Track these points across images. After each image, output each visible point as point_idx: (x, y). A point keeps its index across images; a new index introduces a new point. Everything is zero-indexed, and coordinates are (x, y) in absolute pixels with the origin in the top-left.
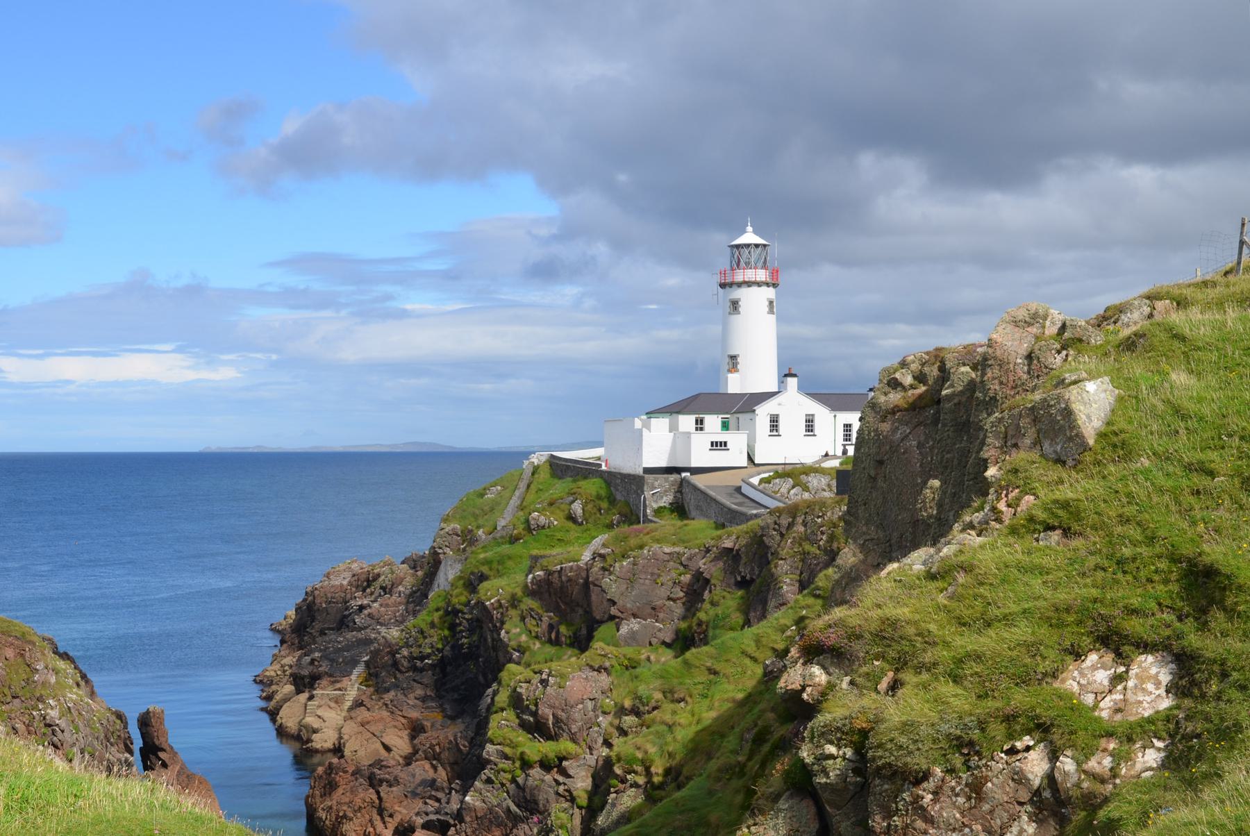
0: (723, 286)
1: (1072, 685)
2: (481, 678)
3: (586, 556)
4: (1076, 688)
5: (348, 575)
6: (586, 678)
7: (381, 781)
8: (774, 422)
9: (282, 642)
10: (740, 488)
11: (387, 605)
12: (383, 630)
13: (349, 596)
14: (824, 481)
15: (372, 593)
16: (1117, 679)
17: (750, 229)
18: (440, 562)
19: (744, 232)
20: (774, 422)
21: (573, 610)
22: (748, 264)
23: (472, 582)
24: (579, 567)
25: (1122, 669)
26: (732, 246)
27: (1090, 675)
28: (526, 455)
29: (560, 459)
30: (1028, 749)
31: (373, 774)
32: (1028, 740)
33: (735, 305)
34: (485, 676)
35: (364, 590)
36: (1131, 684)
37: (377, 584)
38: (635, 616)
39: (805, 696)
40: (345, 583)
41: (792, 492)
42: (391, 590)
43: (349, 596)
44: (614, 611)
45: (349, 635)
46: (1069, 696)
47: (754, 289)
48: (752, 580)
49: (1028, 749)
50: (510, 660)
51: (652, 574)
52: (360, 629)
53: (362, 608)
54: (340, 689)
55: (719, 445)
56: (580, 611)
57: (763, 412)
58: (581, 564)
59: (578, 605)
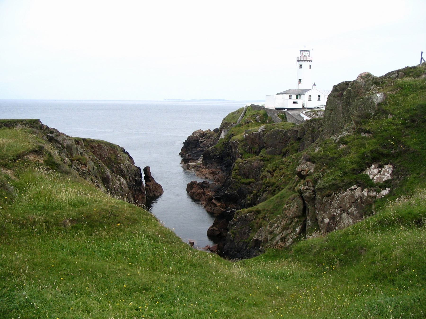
0: (298, 61)
1: (368, 173)
2: (231, 161)
3: (259, 131)
4: (368, 174)
7: (205, 187)
9: (225, 144)
11: (208, 142)
12: (207, 148)
14: (322, 113)
16: (379, 172)
23: (229, 137)
25: (380, 169)
27: (373, 172)
30: (355, 189)
31: (202, 185)
32: (355, 186)
33: (301, 66)
34: (232, 161)
36: (382, 173)
38: (270, 147)
44: (265, 145)
45: (199, 149)
46: (367, 175)
47: (306, 62)
48: (301, 138)
49: (355, 189)
50: (239, 157)
52: (201, 148)
53: (202, 142)
55: (295, 103)
56: (257, 145)
57: (307, 94)
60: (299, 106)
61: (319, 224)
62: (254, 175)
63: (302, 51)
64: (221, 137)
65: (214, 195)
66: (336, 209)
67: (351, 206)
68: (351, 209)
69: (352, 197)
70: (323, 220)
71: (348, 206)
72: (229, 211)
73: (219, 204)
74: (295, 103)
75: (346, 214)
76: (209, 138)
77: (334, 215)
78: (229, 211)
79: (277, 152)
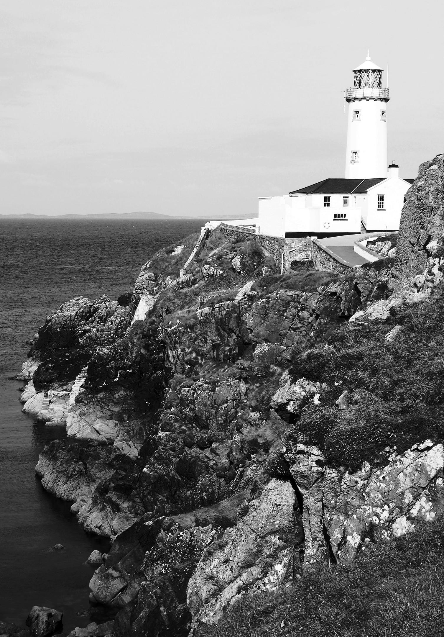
5: (76, 308)
6: (230, 385)
7: (88, 456)
8: (381, 200)
10: (353, 248)
11: (102, 331)
13: (76, 323)
15: (93, 322)
17: (368, 58)
18: (140, 300)
19: (364, 60)
20: (381, 200)
21: (229, 336)
22: (366, 84)
24: (234, 305)
26: (355, 71)
28: (202, 223)
29: (227, 226)
30: (428, 448)
31: (82, 451)
35: (87, 320)
37: (96, 315)
38: (266, 341)
39: (289, 408)
40: (74, 314)
41: (391, 251)
42: (105, 319)
43: (76, 323)
49: (428, 448)
51: (279, 311)
53: (86, 331)
54: (66, 390)
55: (339, 217)
57: (373, 192)
58: (236, 302)
59: (233, 332)
60: (351, 225)
61: (334, 550)
62: (221, 420)
63: (360, 71)
64: (136, 318)
65: (111, 480)
66: (377, 506)
67: (416, 498)
68: (417, 507)
69: (420, 472)
70: (344, 538)
71: (408, 498)
72: (150, 523)
73: (125, 505)
74: (339, 217)
75: (405, 518)
76: (104, 319)
77: (372, 524)
78: (150, 523)
79: (284, 354)
